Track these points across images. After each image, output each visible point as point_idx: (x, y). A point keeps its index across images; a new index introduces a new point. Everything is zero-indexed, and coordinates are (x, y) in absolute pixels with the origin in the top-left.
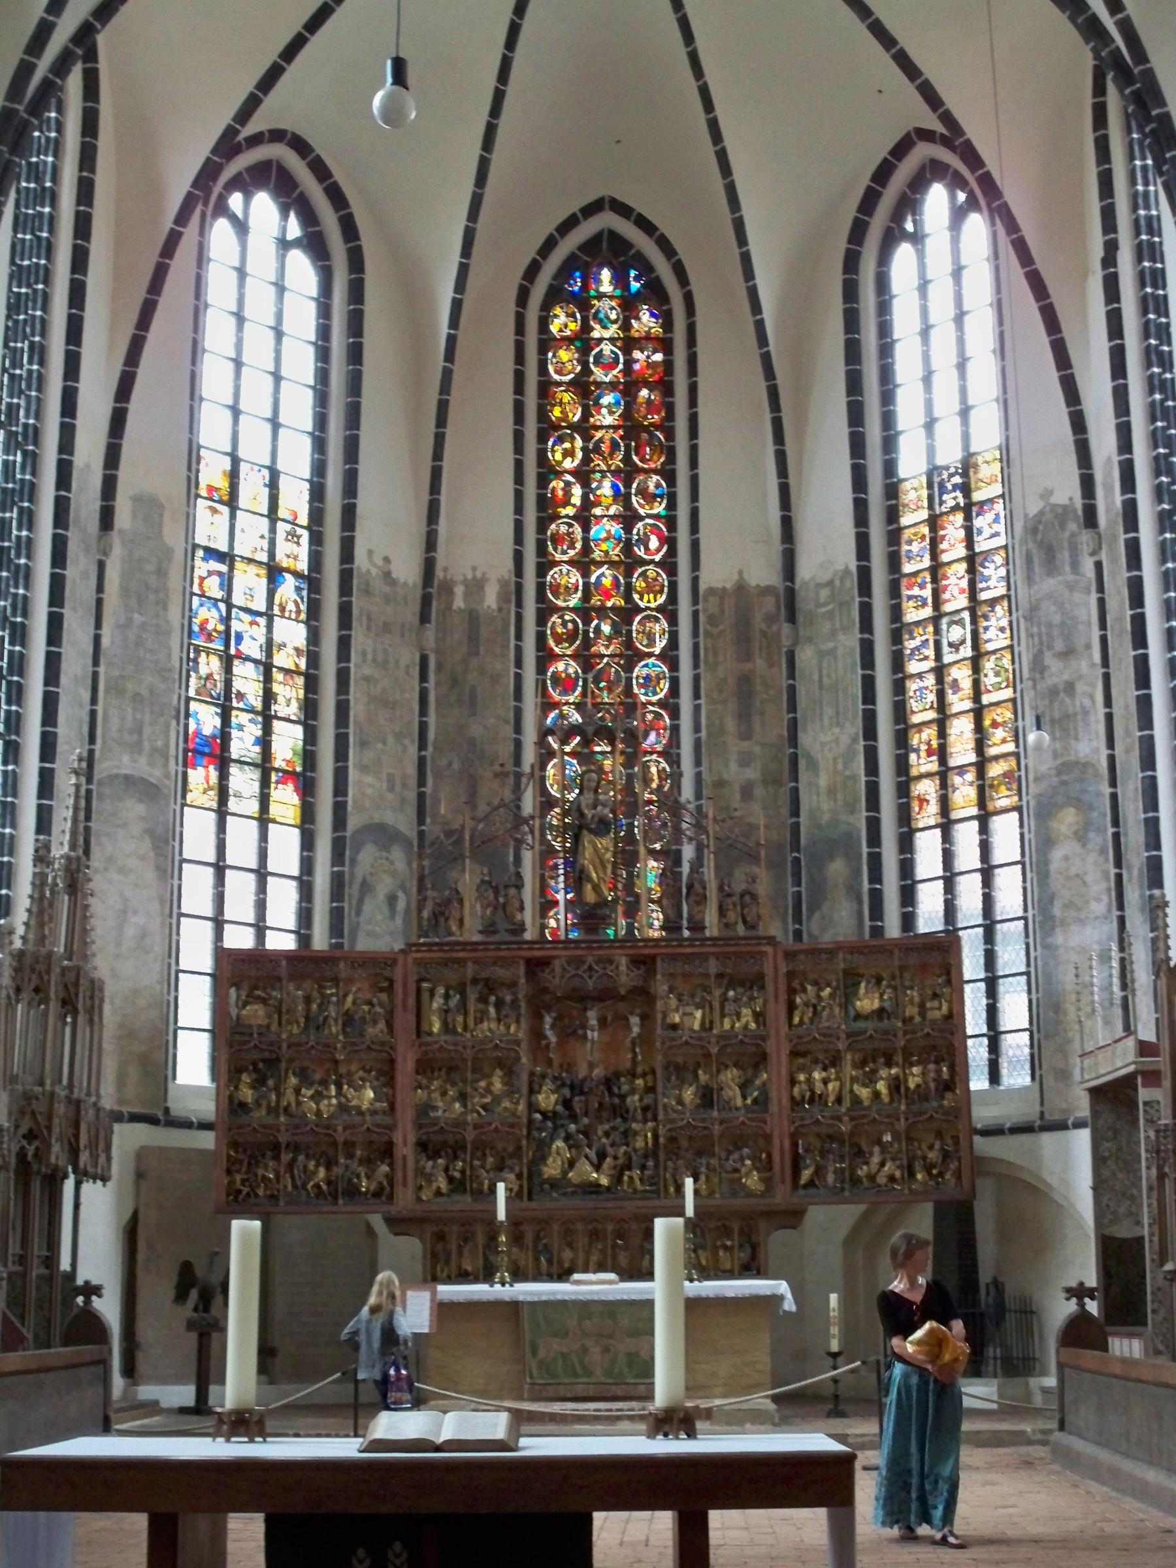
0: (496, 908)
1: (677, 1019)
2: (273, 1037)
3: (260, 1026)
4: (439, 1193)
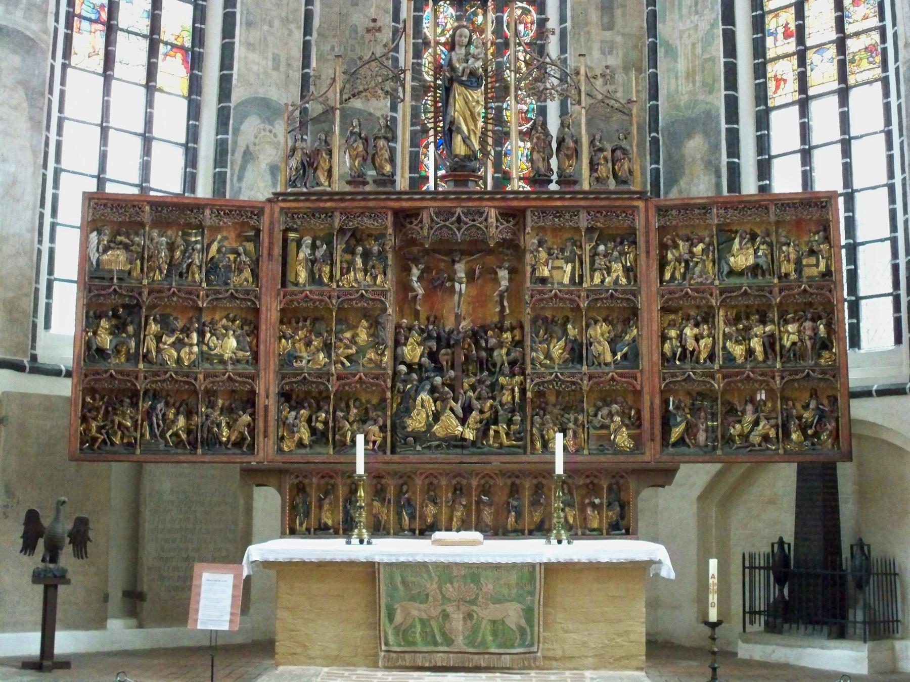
0: (365, 160)
1: (546, 273)
2: (134, 283)
3: (119, 271)
4: (300, 444)
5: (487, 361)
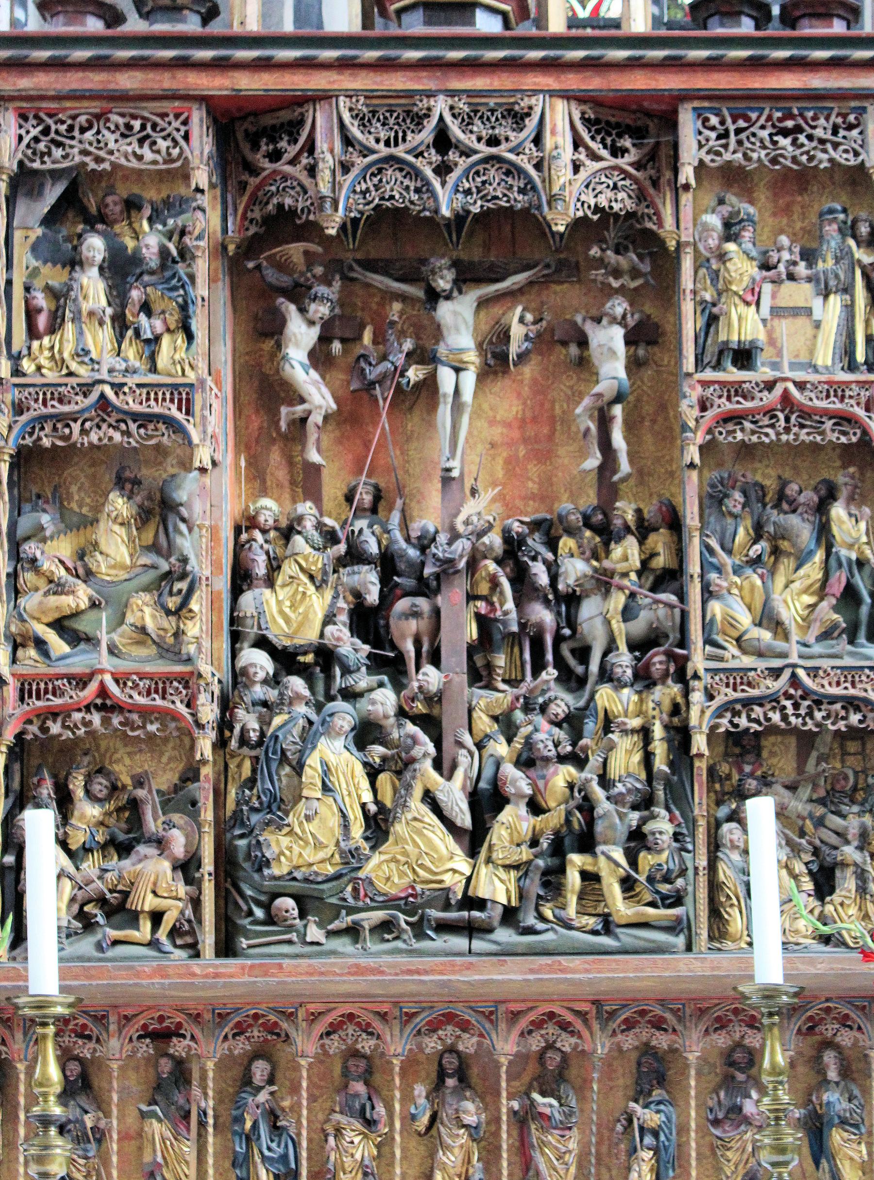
5: (558, 639)
